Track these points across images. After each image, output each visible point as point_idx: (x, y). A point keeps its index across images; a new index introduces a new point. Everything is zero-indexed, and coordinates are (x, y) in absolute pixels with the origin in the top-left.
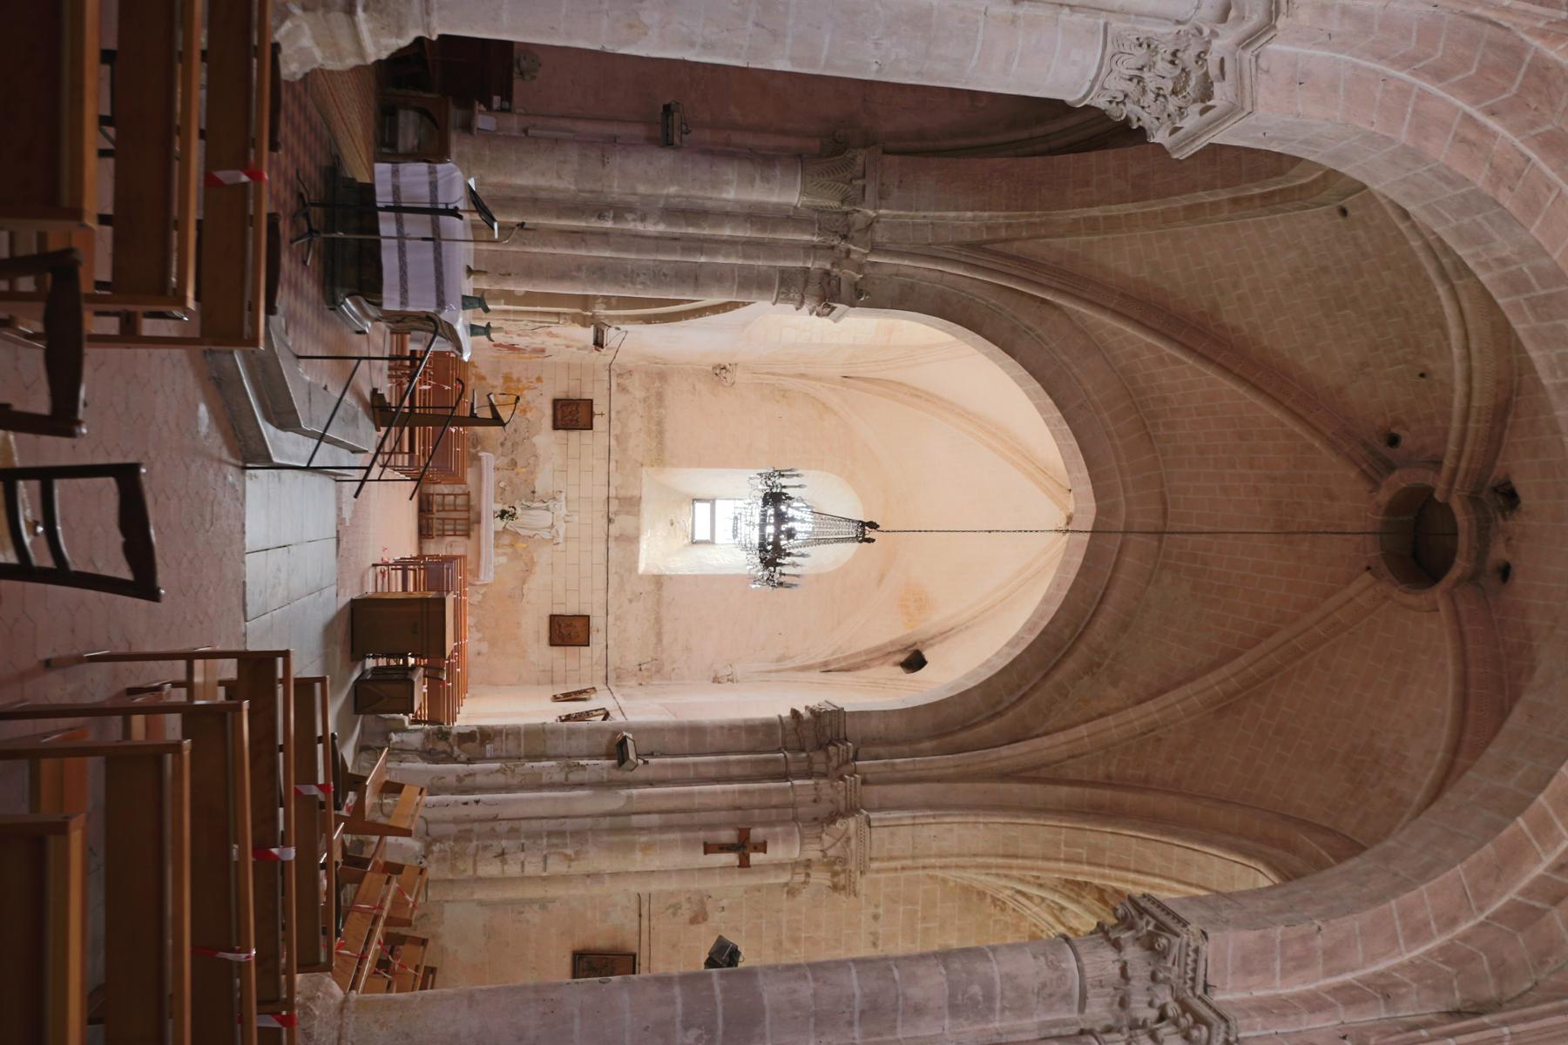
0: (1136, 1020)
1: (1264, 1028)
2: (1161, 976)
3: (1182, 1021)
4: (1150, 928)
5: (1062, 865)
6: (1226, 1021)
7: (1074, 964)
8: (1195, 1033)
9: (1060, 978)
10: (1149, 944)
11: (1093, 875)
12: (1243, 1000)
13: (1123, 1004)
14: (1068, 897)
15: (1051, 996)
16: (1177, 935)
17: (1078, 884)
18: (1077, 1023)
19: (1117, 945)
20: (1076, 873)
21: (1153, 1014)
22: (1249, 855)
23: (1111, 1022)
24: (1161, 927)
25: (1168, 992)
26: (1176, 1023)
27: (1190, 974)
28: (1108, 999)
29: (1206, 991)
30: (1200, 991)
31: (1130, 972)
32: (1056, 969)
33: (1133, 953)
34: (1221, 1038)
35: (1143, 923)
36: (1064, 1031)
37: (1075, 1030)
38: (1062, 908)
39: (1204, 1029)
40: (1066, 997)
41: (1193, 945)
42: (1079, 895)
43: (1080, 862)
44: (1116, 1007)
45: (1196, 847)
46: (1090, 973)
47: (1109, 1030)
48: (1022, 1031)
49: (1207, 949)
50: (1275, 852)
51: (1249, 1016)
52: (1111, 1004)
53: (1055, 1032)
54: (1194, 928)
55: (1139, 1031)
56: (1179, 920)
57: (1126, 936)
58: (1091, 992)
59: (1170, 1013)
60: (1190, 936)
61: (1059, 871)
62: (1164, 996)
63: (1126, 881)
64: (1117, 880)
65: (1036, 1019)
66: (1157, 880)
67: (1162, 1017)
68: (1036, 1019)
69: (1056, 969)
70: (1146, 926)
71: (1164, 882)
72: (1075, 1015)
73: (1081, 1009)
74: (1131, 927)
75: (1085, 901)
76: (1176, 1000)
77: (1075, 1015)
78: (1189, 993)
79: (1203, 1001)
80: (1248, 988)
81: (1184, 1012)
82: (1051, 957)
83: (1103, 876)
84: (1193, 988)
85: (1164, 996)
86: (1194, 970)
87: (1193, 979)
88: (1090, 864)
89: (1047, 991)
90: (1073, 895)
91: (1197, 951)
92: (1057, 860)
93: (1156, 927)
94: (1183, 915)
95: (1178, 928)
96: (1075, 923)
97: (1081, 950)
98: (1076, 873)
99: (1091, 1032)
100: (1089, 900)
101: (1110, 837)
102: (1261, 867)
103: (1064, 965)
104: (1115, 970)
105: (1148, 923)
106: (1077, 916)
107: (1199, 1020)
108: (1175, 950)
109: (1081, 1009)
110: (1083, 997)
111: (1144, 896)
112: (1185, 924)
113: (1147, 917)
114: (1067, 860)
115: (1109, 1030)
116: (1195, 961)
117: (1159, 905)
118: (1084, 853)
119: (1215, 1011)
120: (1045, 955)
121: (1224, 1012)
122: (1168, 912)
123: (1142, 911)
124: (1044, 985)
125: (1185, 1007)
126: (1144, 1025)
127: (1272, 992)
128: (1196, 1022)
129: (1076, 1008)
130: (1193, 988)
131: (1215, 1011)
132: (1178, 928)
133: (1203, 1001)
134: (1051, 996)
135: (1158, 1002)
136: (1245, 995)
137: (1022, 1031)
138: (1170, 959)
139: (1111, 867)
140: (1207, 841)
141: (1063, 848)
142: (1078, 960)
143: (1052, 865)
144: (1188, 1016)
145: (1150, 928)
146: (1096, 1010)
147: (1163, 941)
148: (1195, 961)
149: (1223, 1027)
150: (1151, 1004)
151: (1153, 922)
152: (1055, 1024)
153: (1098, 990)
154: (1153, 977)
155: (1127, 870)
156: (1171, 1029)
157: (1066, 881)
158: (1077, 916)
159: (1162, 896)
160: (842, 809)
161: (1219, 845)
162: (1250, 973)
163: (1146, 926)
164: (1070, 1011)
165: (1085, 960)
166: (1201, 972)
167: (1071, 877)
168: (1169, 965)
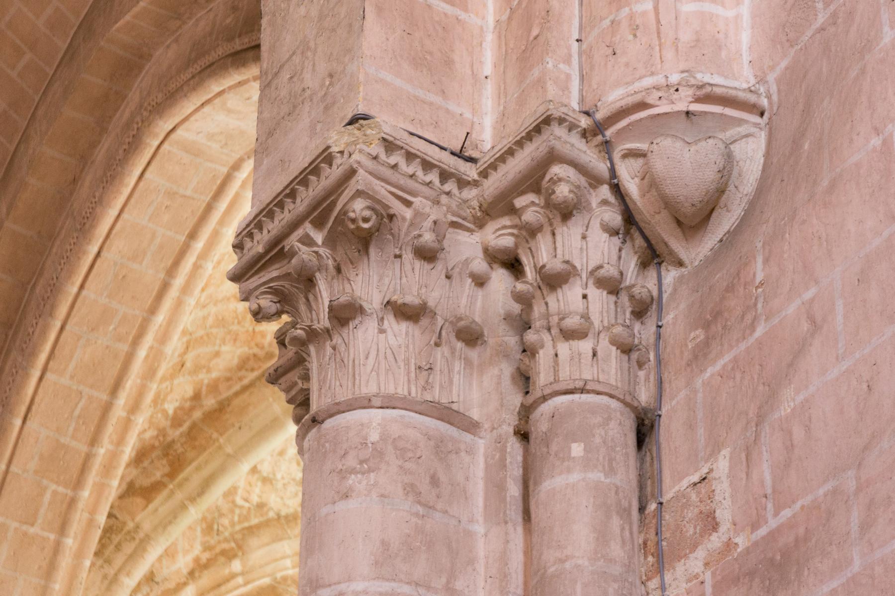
0: (508, 318)
1: (568, 60)
2: (428, 238)
3: (530, 216)
4: (319, 237)
5: (70, 542)
6: (547, 121)
7: (376, 416)
8: (563, 191)
9: (401, 452)
10: (360, 241)
11: (100, 489)
12: (501, 93)
13: (471, 336)
14: (133, 558)
15: (434, 481)
16: (351, 173)
17: (108, 531)
18: (500, 441)
19: (345, 314)
20: (91, 523)
21: (500, 279)
22: (133, 145)
23: (507, 370)
24: (319, 213)
25: (463, 236)
26: (532, 232)
27: (433, 177)
28: (458, 366)
29: (471, 160)
30: (471, 172)
31: (411, 299)
32: (379, 454)
33: (373, 282)
34: (575, 139)
35: (305, 253)
36: (515, 471)
37: (514, 447)
38: (150, 578)
39: (557, 170)
40: (442, 450)
41: (377, 149)
42: (130, 536)
43: (72, 503)
44: (474, 354)
45: (93, 249)
46: (399, 386)
47: (524, 379)
48: (504, 559)
49: (389, 123)
50: (134, 97)
51: (540, 83)
52: (468, 363)
53: (514, 490)
54: (338, 139)
55: (538, 309)
56: (314, 169)
57: (326, 292)
58: (436, 394)
59: (507, 241)
60: (358, 150)
61: (79, 555)
62: (467, 248)
63: (127, 424)
64: (120, 441)
65: (479, 528)
66: (142, 353)
67: (514, 266)
68: (479, 528)
69: (379, 454)
70: (311, 246)
71: (149, 340)
72: (482, 444)
73: (471, 427)
74: (308, 281)
75: (146, 526)
76: (480, 224)
77: (482, 444)
78: (470, 194)
79: (493, 166)
80: (477, 80)
81: (513, 211)
82: (351, 461)
83: (108, 469)
84: (462, 183)
85: (467, 248)
86: (427, 165)
87: (445, 176)
88: (78, 484)
89: (424, 486)
90: (128, 548)
91: (390, 146)
92: (57, 548)
93: (319, 224)
94: (301, 161)
95: (331, 174)
96: (184, 563)
97: (343, 395)
98: (91, 523)
99: (526, 412)
100: (145, 517)
101: (32, 424)
102: (164, 125)
103: (374, 437)
104: (399, 331)
105: (307, 241)
106: (170, 554)
107: (534, 180)
108: (382, 190)
109: (471, 427)
110: (447, 414)
111: (238, 246)
112: (326, 157)
113: (293, 241)
114: (62, 530)
115: (524, 379)
116: (410, 156)
117: (267, 212)
118: (54, 488)
119: (520, 143)
120: (343, 474)
121: (528, 121)
122: (278, 203)
123: (276, 252)
124: (411, 489)
125: (501, 206)
126: (525, 300)
127: (490, 38)
128: (537, 190)
129: (468, 437)
130: (462, 183)
131: (520, 143)
132: (331, 174)
133: (493, 166)
134: (434, 481)
135: (480, 265)
136: (489, 90)
137: (504, 559)
138: (397, 207)
139: (94, 441)
140: (84, 226)
141: (32, 530)
142: (366, 403)
143: (65, 562)
144: (519, 202)
145: (319, 237)
146: (475, 395)
147: (359, 207)
148: (410, 156)
149: (559, 131)
150: (480, 281)
151: (307, 227)
152: (496, 487)
153: (437, 378)
154: (428, 255)
155: (107, 408)
156: (543, 244)
157: (97, 554)
158: (170, 554)
159: (246, 210)
160: (43, 582)
161: (98, 202)
162: (449, 63)
163: (311, 246)
164: (470, 451)
165: (369, 388)
166: (434, 154)
167: (93, 545)
168: (408, 213)
